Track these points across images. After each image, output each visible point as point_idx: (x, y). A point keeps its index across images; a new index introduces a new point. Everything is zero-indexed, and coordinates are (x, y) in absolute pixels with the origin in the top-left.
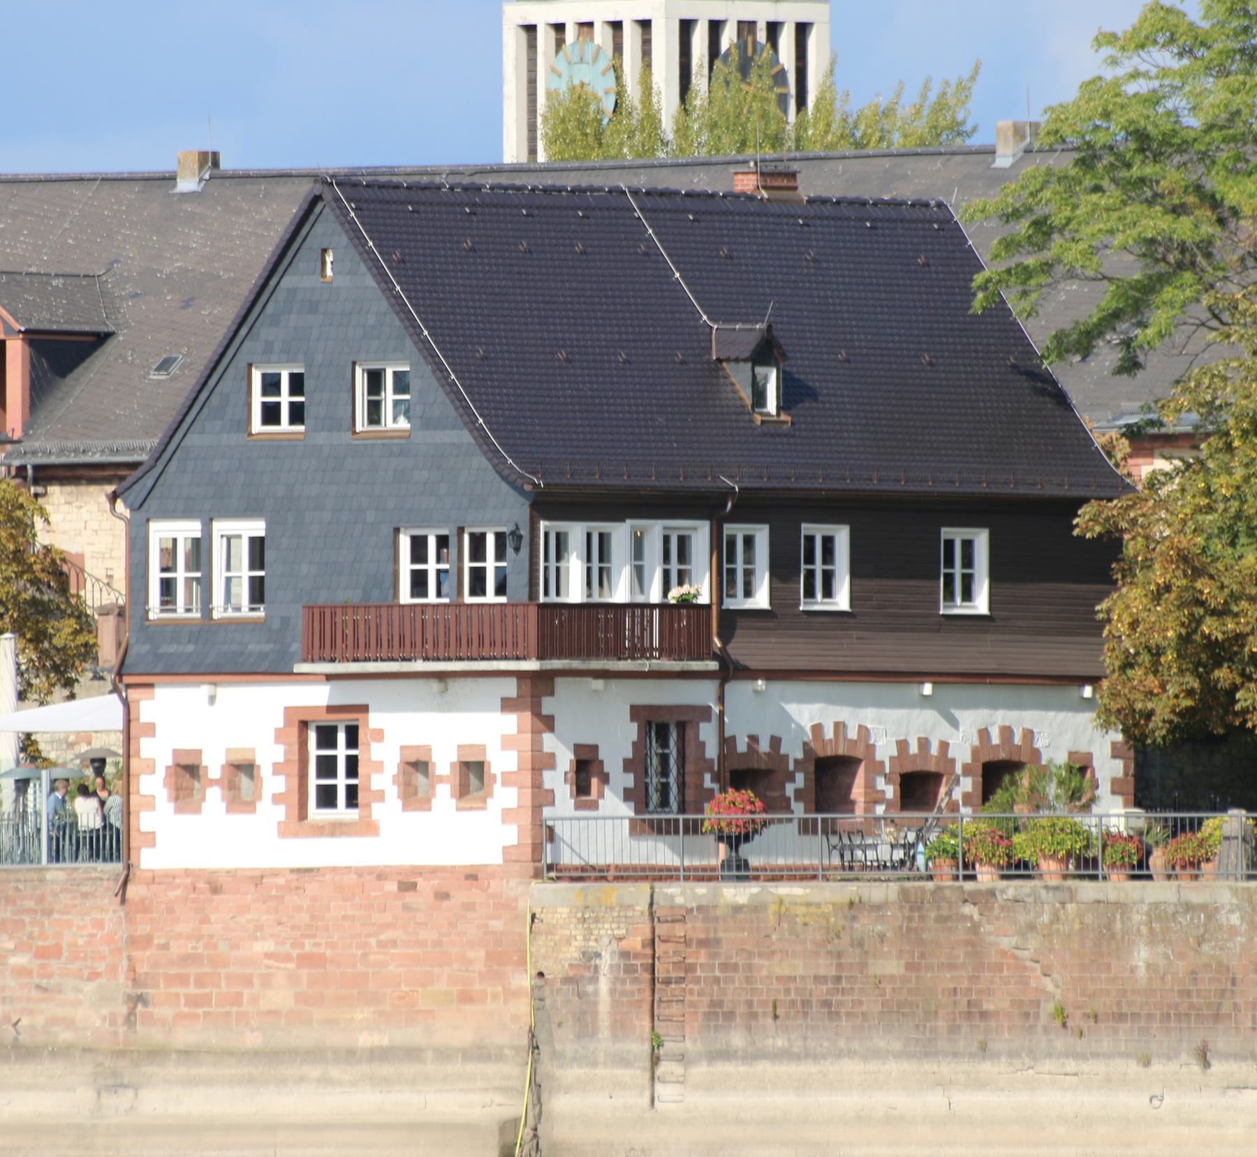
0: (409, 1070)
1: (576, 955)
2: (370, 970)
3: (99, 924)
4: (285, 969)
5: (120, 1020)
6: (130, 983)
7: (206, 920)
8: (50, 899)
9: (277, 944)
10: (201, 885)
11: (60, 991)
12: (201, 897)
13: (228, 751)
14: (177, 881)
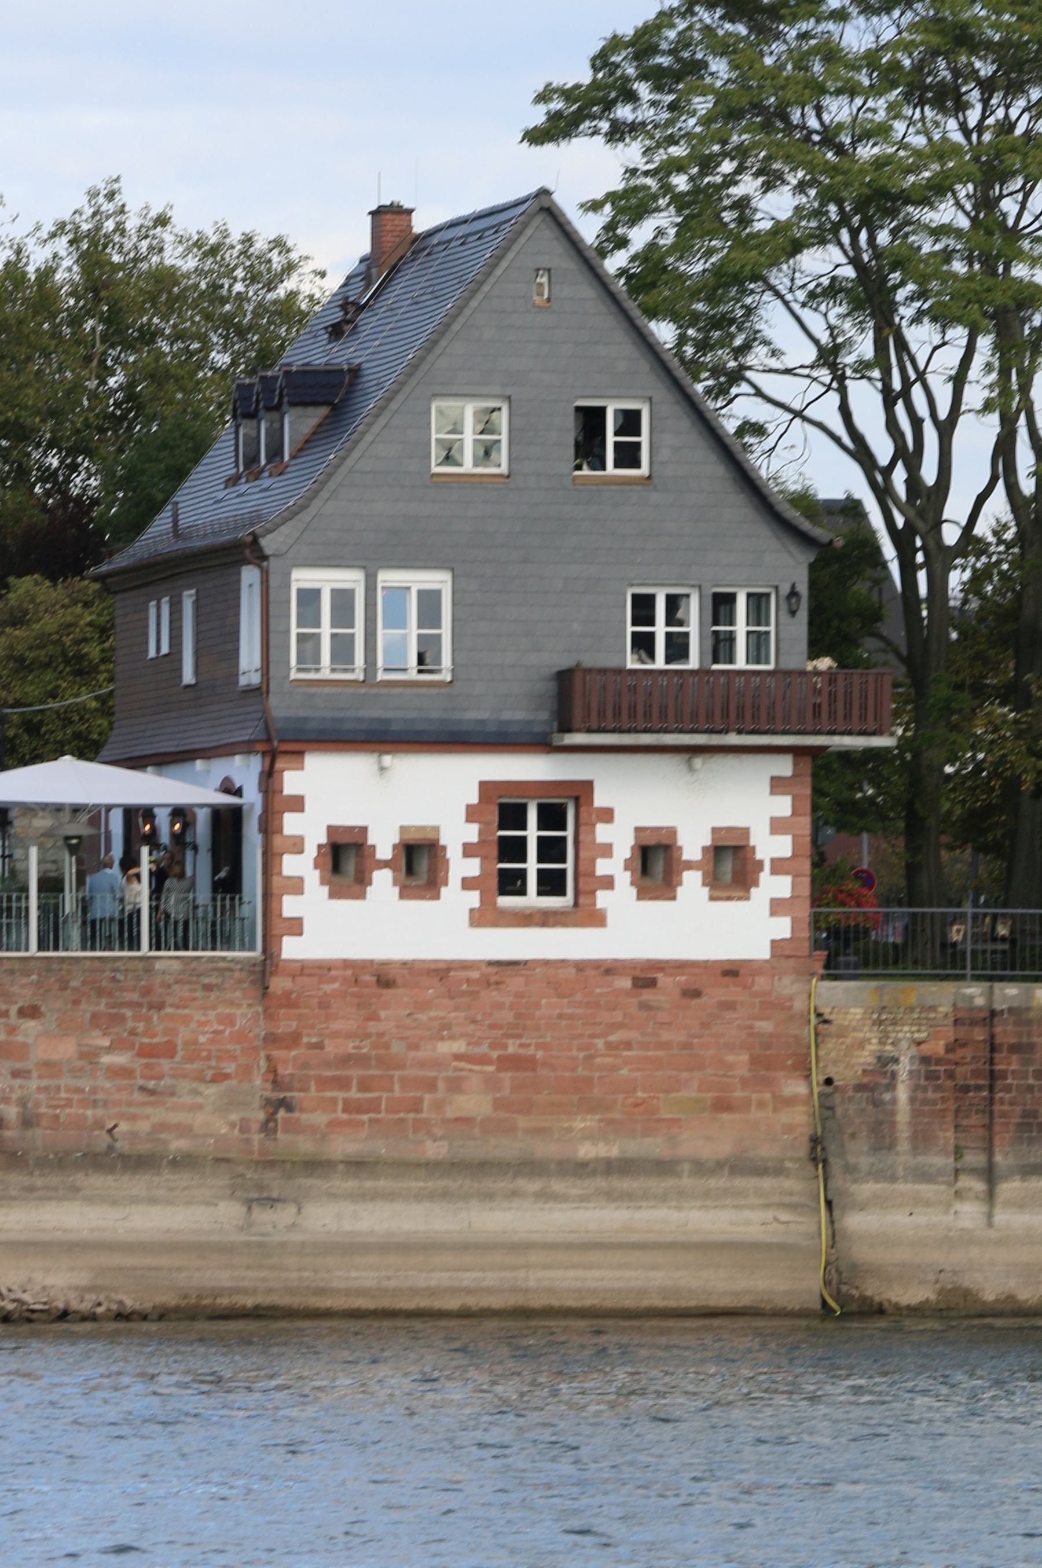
0: (654, 1184)
1: (871, 1060)
2: (597, 1074)
3: (230, 1020)
4: (480, 1072)
5: (255, 1127)
6: (269, 1085)
7: (374, 1017)
8: (160, 991)
9: (469, 1044)
10: (368, 978)
11: (173, 1094)
12: (366, 991)
13: (403, 829)
14: (333, 973)
